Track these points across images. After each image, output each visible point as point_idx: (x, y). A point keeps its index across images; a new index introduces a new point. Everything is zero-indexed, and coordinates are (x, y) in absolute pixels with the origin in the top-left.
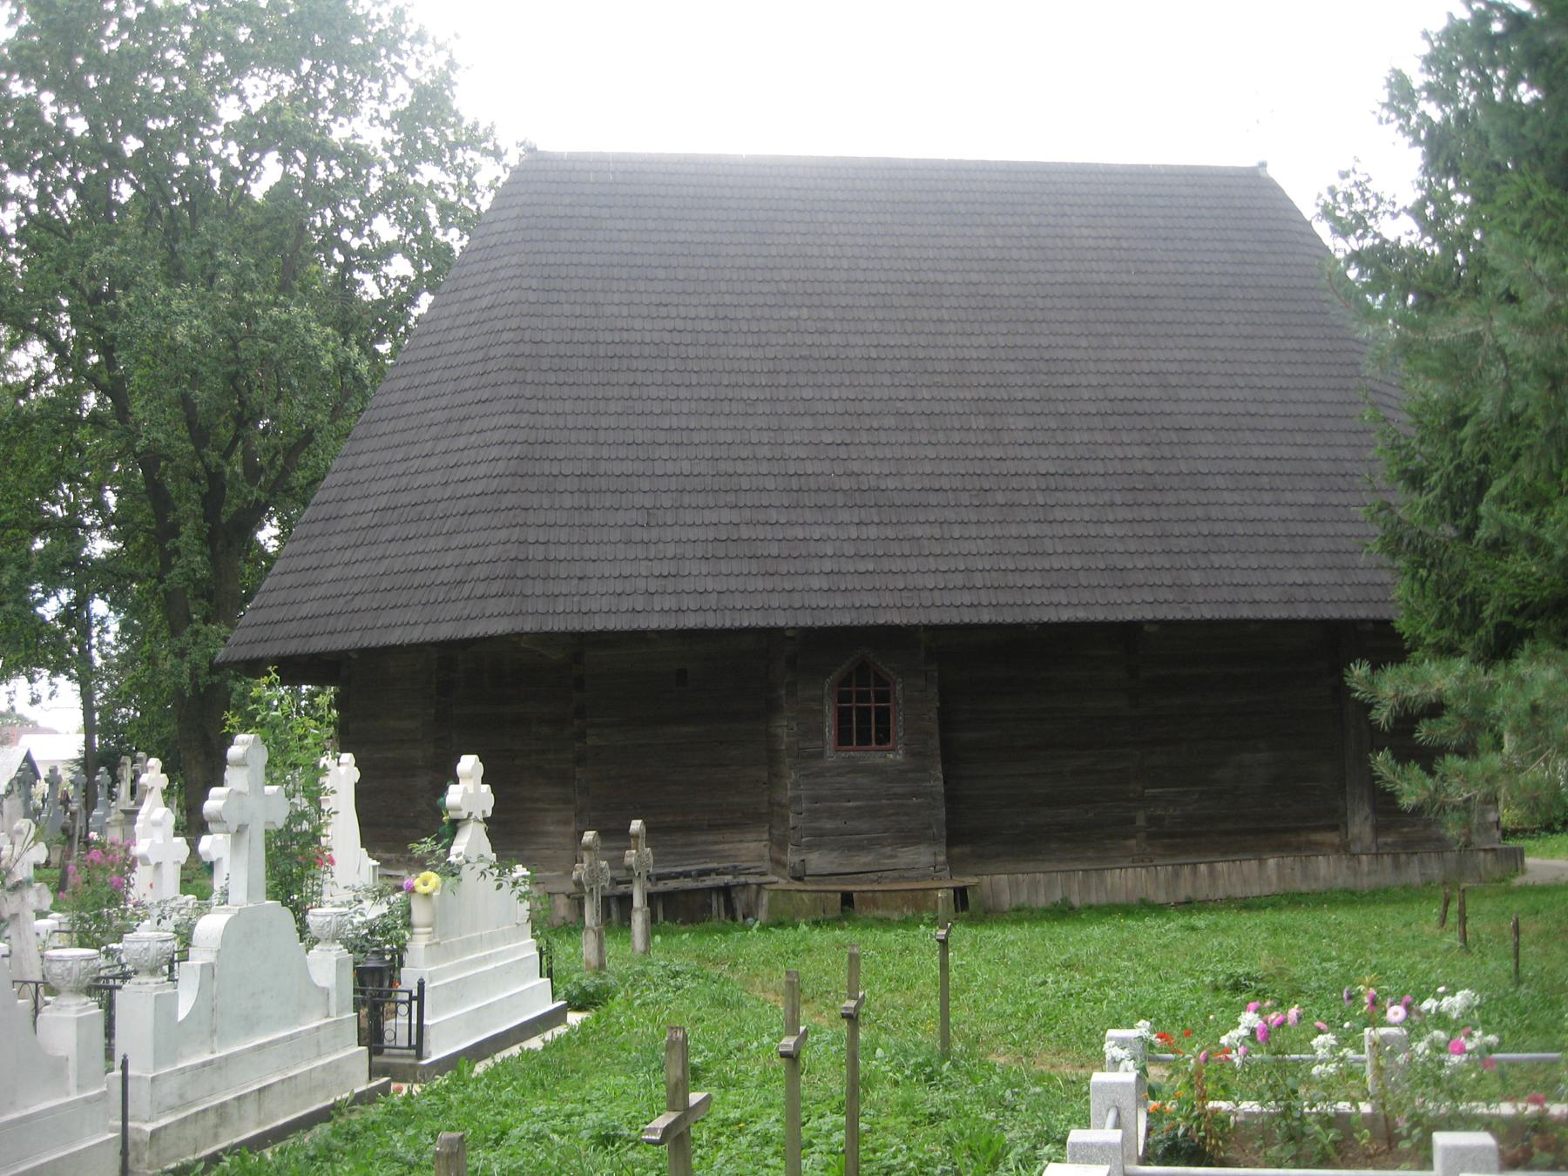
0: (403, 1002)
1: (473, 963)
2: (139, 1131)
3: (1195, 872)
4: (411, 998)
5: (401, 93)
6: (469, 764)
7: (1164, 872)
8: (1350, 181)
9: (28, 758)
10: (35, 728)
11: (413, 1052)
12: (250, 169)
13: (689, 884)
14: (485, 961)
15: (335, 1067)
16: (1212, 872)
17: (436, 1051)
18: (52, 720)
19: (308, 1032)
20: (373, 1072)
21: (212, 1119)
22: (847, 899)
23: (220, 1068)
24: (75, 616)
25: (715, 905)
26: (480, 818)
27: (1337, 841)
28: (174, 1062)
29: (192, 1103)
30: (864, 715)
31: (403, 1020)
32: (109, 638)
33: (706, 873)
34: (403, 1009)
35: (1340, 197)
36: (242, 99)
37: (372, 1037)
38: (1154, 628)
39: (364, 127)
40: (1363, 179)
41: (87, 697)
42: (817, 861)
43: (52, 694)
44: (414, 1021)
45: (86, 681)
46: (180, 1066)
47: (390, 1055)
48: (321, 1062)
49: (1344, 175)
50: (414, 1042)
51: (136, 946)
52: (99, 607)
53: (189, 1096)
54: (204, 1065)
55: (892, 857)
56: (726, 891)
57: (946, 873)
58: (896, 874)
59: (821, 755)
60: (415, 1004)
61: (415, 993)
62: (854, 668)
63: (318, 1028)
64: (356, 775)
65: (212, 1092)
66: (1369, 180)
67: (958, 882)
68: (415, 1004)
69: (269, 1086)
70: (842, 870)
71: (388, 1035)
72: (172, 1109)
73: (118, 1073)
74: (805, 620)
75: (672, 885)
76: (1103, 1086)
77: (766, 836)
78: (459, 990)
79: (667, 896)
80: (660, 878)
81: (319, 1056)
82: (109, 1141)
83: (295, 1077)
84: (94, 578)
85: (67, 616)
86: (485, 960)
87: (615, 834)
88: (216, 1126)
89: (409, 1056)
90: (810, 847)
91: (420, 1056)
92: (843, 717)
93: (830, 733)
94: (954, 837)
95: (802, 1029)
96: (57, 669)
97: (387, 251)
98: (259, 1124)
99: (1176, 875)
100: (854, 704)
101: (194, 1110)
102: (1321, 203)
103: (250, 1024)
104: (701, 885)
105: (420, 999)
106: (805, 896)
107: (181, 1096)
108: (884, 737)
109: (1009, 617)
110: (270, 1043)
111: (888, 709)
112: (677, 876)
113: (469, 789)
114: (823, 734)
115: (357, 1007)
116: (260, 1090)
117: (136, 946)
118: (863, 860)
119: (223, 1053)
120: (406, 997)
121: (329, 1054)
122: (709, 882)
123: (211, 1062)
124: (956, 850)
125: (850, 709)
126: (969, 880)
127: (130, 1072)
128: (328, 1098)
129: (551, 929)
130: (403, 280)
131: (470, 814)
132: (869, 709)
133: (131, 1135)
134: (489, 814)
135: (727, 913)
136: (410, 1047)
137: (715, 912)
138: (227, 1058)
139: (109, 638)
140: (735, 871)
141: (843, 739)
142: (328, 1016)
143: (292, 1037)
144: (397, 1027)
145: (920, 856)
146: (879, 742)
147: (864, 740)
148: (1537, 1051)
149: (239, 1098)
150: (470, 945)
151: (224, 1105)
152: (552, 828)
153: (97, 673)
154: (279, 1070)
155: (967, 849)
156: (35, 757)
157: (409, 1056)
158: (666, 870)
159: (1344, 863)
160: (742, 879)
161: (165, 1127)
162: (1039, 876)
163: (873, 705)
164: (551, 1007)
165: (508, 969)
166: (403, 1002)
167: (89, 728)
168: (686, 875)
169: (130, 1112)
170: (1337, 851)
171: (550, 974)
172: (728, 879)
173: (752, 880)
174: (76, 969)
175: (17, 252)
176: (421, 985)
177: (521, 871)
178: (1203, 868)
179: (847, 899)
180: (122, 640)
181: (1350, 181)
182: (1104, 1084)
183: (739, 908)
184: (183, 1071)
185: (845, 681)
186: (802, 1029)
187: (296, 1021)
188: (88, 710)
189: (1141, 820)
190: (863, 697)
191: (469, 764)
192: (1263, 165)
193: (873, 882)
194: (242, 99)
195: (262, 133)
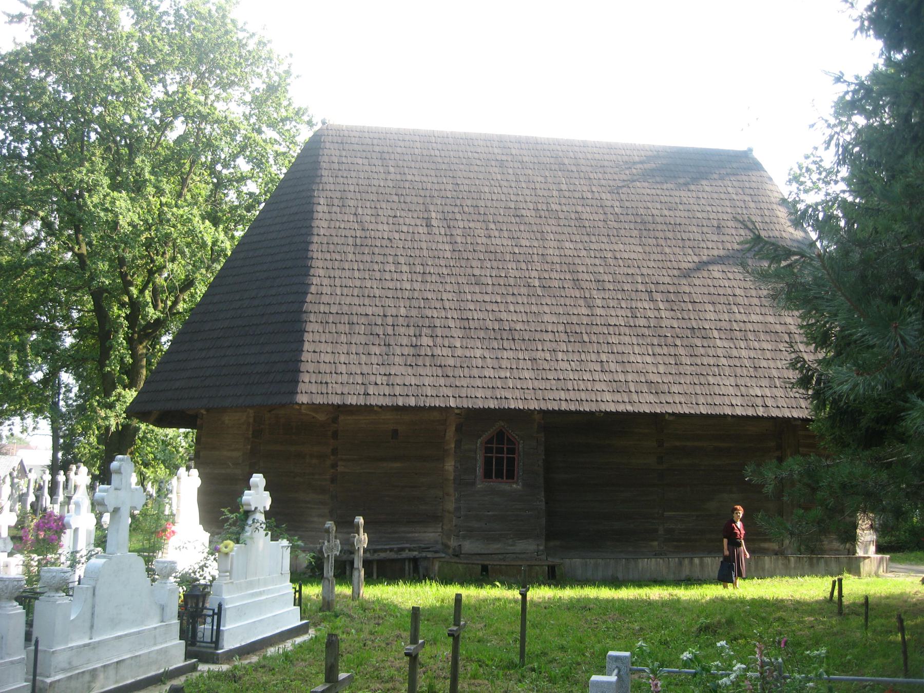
0: (209, 616)
1: (253, 595)
2: (43, 682)
3: (691, 562)
4: (214, 614)
5: (258, 84)
6: (258, 479)
7: (674, 561)
8: (810, 160)
9: (21, 463)
10: (27, 446)
11: (213, 645)
12: (164, 126)
13: (393, 555)
14: (263, 596)
15: (165, 651)
16: (702, 564)
17: (230, 643)
18: (34, 441)
19: (149, 630)
20: (188, 656)
21: (87, 678)
22: (485, 568)
23: (94, 648)
24: (51, 380)
25: (407, 568)
26: (262, 510)
27: (776, 547)
28: (67, 643)
29: (76, 668)
30: (499, 461)
31: (208, 626)
32: (72, 395)
33: (402, 549)
34: (209, 620)
35: (804, 170)
36: (165, 86)
37: (188, 634)
38: (672, 418)
39: (232, 106)
40: (818, 159)
41: (55, 431)
42: (469, 546)
43: (34, 428)
44: (215, 628)
45: (56, 418)
46: (70, 645)
47: (200, 646)
48: (156, 648)
49: (807, 157)
50: (214, 639)
51: (48, 574)
52: (66, 377)
53: (75, 663)
54: (85, 646)
55: (512, 545)
56: (415, 561)
57: (544, 557)
58: (514, 556)
59: (473, 484)
60: (216, 617)
61: (216, 611)
62: (498, 437)
63: (155, 628)
64: (198, 482)
65: (89, 662)
66: (821, 161)
67: (552, 561)
68: (216, 617)
69: (123, 661)
70: (483, 552)
71: (200, 635)
72: (64, 670)
73: (33, 648)
74: (466, 404)
75: (383, 555)
76: (597, 683)
77: (440, 530)
78: (241, 611)
79: (381, 562)
80: (375, 551)
81: (155, 644)
82: (24, 687)
83: (140, 656)
84: (59, 361)
85: (45, 381)
86: (261, 593)
87: (346, 526)
88: (90, 682)
89: (211, 648)
90: (464, 537)
91: (217, 648)
92: (488, 462)
93: (480, 471)
94: (551, 535)
95: (420, 641)
96: (39, 412)
97: (242, 179)
98: (116, 682)
99: (680, 564)
100: (494, 455)
101: (77, 672)
102: (792, 173)
103: (114, 623)
104: (399, 557)
105: (219, 614)
106: (460, 566)
107: (70, 663)
108: (511, 476)
109: (586, 407)
110: (126, 635)
111: (514, 458)
112: (385, 550)
113: (258, 496)
114: (476, 470)
115: (180, 616)
116: (117, 662)
117: (48, 574)
118: (495, 547)
119: (97, 639)
120: (211, 613)
121: (161, 643)
122: (405, 554)
123: (88, 645)
124: (552, 544)
125: (492, 457)
126: (557, 561)
127: (40, 648)
128: (159, 669)
129: (300, 576)
130: (251, 194)
131: (256, 508)
132: (492, 457)
133: (37, 683)
134: (268, 508)
135: (414, 572)
136: (212, 642)
137: (407, 572)
138: (99, 642)
139: (72, 395)
140: (422, 550)
141: (487, 475)
142: (162, 621)
143: (139, 633)
144: (205, 629)
145: (529, 546)
146: (497, 477)
147: (499, 475)
148: (889, 676)
149: (104, 666)
150: (251, 585)
151: (95, 670)
152: (316, 519)
153: (62, 416)
154: (130, 651)
155: (557, 543)
156: (25, 464)
157: (211, 648)
158: (380, 547)
159: (780, 562)
160: (424, 554)
161: (59, 681)
162: (600, 561)
163: (505, 456)
164: (299, 623)
165: (274, 600)
166: (209, 616)
167: (56, 448)
168: (391, 550)
169: (38, 671)
170: (776, 554)
171: (300, 605)
172: (415, 553)
173: (429, 555)
174: (11, 586)
175: (29, 168)
176: (220, 606)
177: (285, 542)
178: (686, 561)
179: (485, 568)
180: (80, 397)
181: (810, 160)
182: (597, 682)
183: (421, 571)
184: (72, 648)
185: (490, 441)
186: (420, 641)
187: (142, 623)
188: (55, 437)
189: (661, 532)
190: (500, 451)
191: (258, 479)
192: (750, 150)
193: (500, 560)
194: (165, 86)
195: (172, 107)
